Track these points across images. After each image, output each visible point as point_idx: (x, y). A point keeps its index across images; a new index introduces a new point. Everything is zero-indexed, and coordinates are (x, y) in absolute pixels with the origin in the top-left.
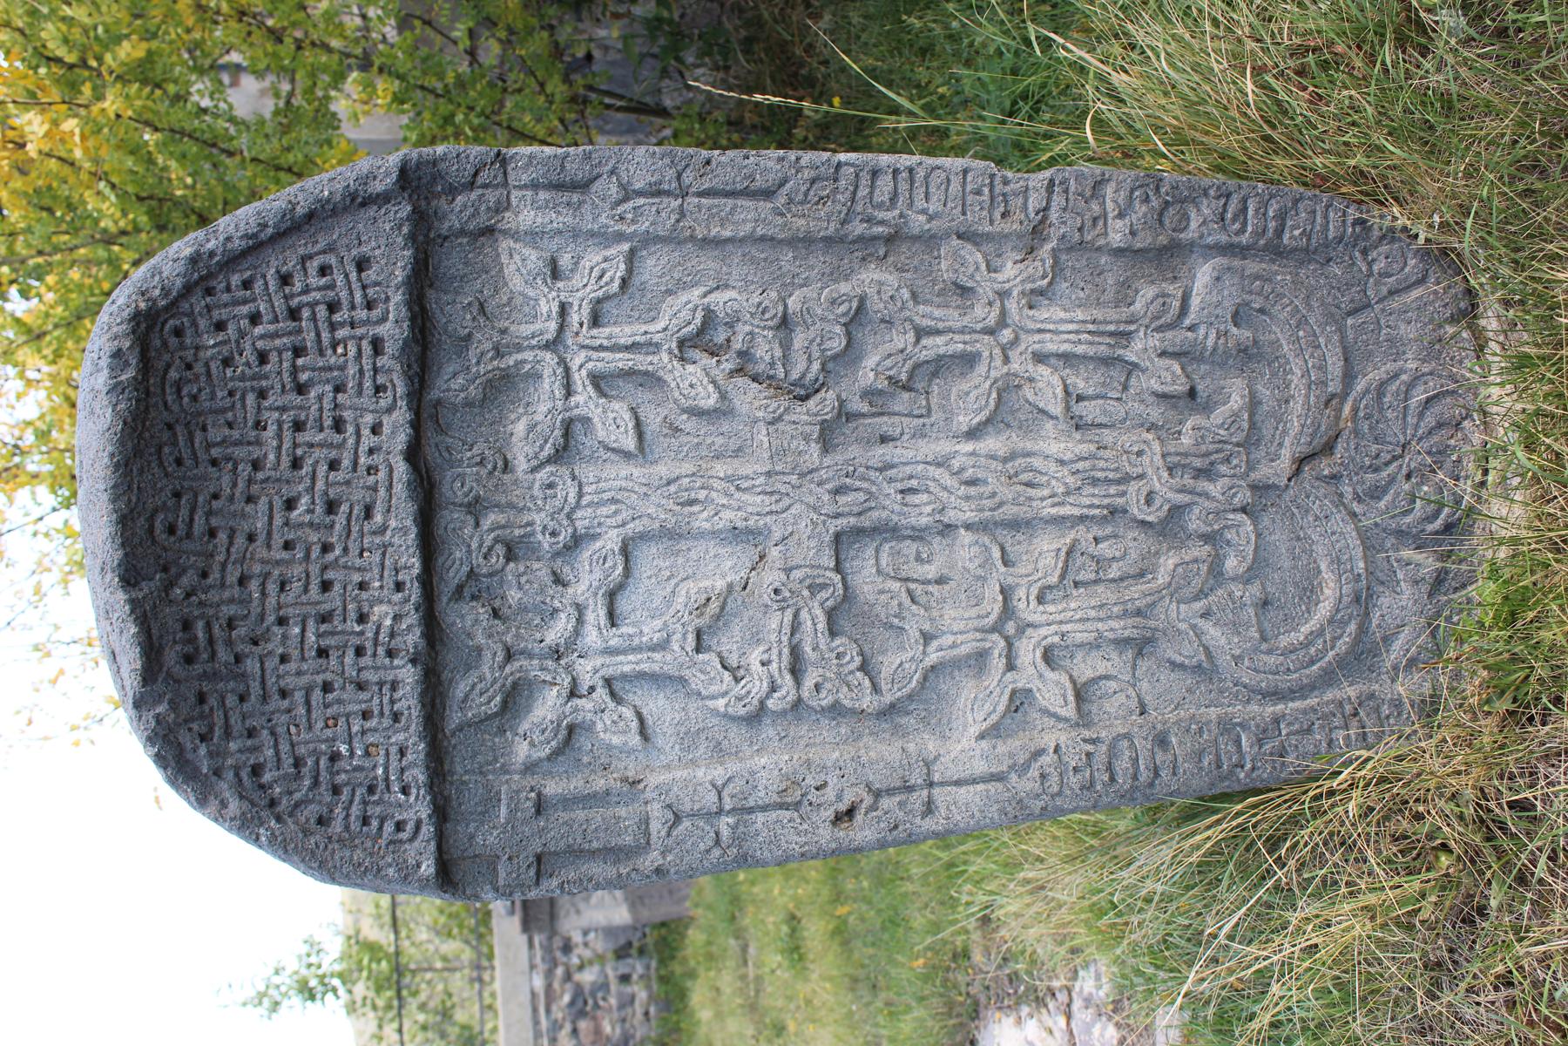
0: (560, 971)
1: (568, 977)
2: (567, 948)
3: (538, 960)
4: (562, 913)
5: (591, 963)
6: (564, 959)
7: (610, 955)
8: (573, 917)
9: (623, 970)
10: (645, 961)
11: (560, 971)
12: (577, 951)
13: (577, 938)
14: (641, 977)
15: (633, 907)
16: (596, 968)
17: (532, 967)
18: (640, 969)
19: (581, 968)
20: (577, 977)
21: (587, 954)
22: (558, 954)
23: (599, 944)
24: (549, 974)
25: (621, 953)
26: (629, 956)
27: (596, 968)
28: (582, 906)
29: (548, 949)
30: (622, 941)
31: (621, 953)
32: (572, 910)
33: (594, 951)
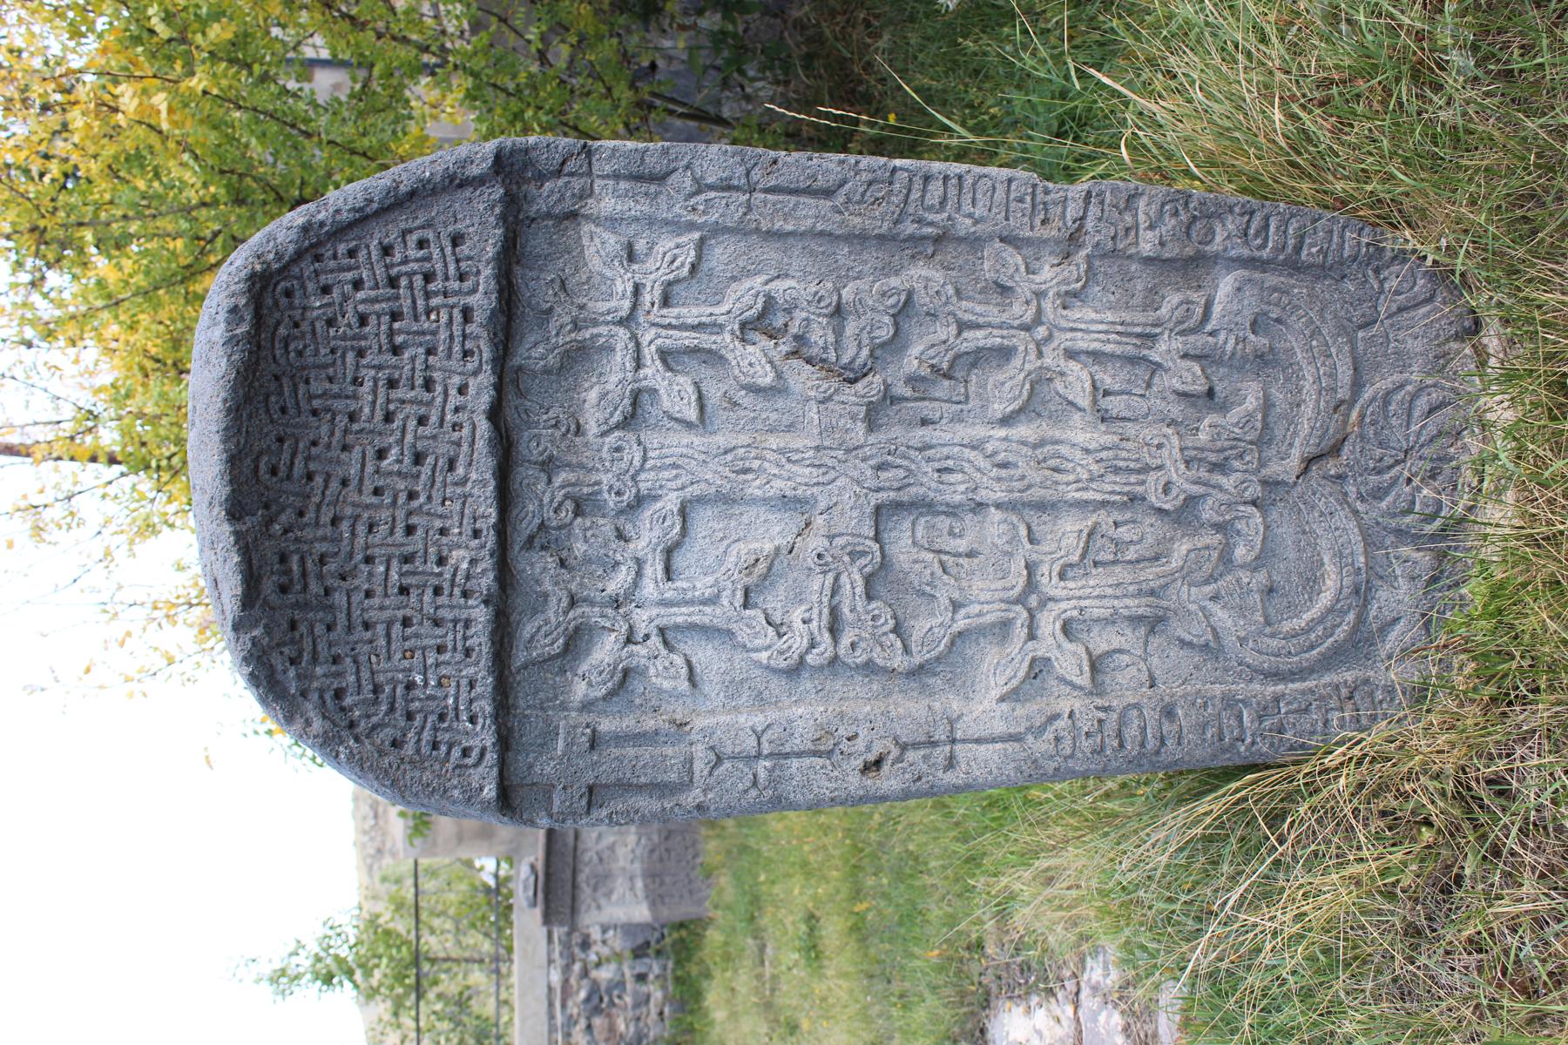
0: (577, 967)
1: (585, 973)
2: (586, 944)
3: (556, 955)
4: (583, 908)
5: (608, 960)
6: (583, 956)
7: (627, 954)
8: (594, 912)
9: (640, 969)
10: (662, 962)
11: (577, 967)
12: (595, 948)
13: (596, 934)
14: (657, 977)
15: (653, 905)
16: (613, 966)
17: (550, 962)
18: (656, 969)
19: (598, 965)
20: (594, 974)
21: (605, 951)
22: (577, 950)
23: (617, 942)
24: (567, 969)
25: (639, 953)
26: (647, 955)
27: (613, 966)
28: (603, 901)
29: (566, 945)
30: (640, 941)
31: (639, 953)
32: (594, 905)
33: (612, 949)
